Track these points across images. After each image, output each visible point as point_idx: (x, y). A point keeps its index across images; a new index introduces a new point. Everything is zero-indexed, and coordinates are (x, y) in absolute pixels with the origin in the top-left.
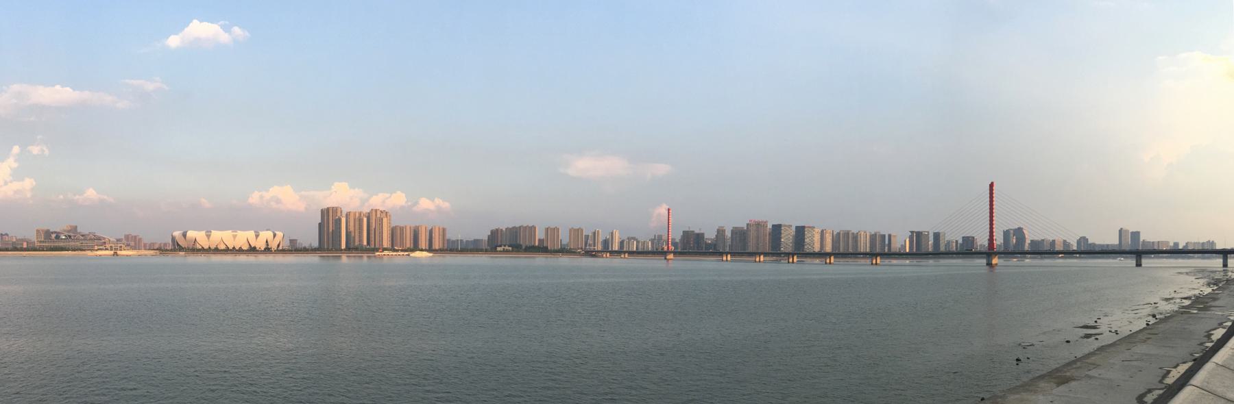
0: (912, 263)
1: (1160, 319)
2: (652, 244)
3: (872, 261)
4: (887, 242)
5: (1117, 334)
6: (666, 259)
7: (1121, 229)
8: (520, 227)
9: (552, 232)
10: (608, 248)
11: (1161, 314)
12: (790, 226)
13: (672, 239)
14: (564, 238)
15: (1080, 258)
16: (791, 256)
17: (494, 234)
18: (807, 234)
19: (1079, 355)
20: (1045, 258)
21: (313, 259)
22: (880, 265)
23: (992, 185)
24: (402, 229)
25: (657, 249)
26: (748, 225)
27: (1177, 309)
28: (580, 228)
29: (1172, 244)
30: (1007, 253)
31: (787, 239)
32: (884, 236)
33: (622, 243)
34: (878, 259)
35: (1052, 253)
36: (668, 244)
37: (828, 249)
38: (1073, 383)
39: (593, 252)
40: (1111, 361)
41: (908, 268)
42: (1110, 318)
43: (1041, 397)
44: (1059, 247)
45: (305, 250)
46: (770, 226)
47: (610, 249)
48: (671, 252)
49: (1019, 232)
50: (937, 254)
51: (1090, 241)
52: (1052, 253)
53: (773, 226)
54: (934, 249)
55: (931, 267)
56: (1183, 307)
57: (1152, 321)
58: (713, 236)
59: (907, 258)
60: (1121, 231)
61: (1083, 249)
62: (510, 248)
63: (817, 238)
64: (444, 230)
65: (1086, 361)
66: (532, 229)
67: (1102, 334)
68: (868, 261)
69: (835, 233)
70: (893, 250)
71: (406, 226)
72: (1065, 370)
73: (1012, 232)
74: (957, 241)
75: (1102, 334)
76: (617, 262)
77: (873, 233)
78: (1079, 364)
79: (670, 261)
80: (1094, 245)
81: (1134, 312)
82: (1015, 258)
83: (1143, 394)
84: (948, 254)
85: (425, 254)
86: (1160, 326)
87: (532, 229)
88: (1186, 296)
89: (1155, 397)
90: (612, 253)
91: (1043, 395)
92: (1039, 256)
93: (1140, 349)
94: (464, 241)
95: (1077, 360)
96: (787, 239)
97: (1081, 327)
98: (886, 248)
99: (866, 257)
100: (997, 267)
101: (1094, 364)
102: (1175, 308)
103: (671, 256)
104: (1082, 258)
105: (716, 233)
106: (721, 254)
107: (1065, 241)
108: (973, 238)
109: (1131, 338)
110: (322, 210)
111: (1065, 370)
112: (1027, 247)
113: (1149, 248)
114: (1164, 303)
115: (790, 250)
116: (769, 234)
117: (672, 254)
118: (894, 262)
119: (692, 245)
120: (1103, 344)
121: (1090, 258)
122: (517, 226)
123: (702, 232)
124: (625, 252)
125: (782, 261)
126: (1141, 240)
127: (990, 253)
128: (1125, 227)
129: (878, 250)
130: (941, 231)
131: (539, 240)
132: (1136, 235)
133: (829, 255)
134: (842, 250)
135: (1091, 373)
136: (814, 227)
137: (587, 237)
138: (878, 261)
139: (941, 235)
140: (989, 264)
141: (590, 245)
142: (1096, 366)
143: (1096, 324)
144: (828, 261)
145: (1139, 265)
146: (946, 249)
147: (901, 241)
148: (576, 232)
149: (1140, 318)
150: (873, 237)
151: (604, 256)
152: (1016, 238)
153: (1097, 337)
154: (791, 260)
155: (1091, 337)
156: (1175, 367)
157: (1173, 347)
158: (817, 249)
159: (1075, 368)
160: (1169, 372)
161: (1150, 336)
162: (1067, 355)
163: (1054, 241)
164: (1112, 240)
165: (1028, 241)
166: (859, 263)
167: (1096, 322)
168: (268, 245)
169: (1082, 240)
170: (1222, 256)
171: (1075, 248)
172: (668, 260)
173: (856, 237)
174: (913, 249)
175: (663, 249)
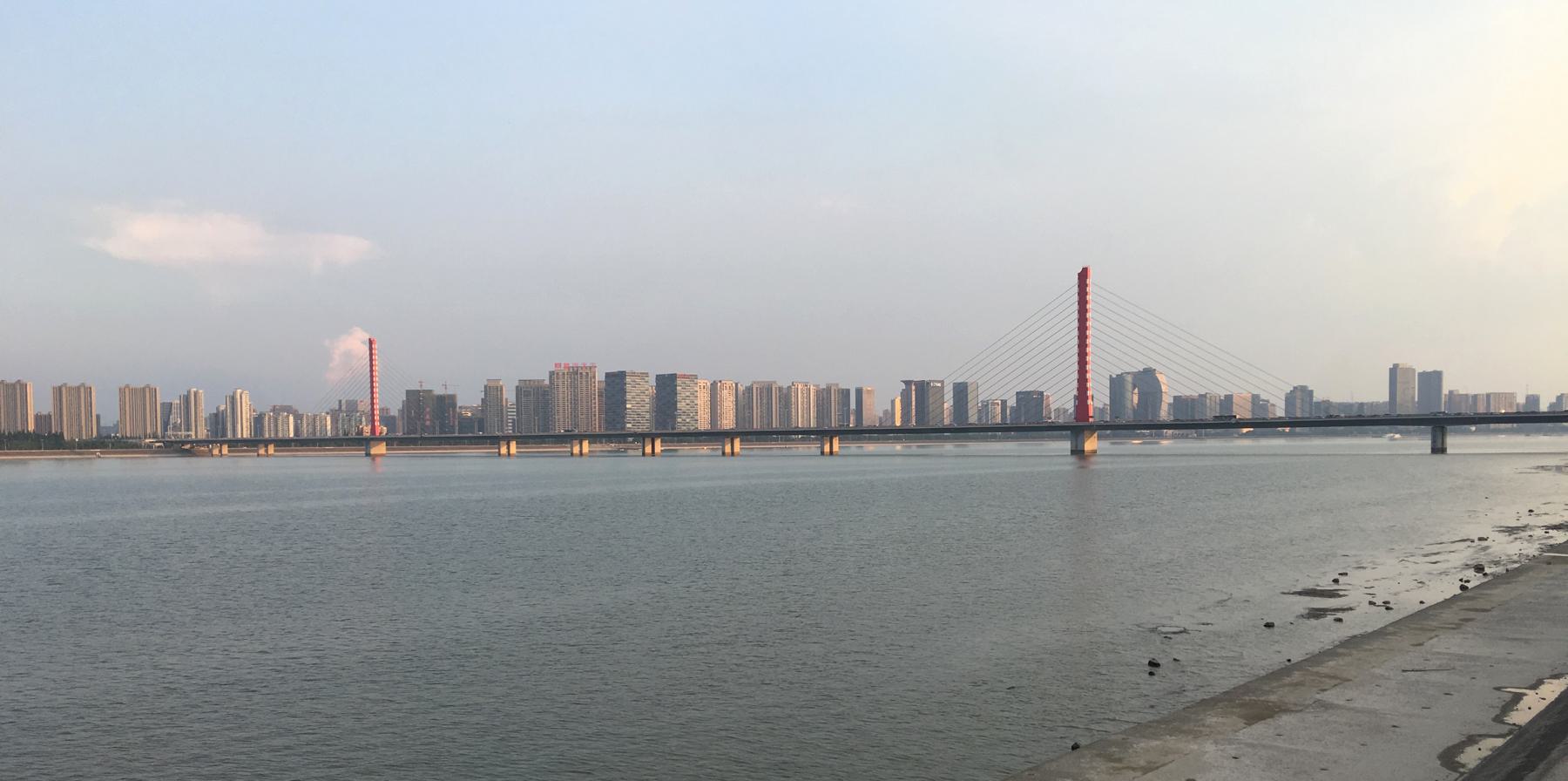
0: (908, 451)
1: (1496, 576)
2: (335, 421)
3: (822, 448)
4: (853, 406)
5: (1387, 608)
6: (368, 455)
9: (72, 396)
10: (224, 434)
11: (1497, 563)
13: (382, 410)
14: (107, 410)
16: (648, 441)
19: (1296, 657)
20: (1207, 435)
23: (1083, 276)
25: (345, 434)
26: (552, 374)
27: (1536, 553)
28: (148, 386)
29: (1521, 400)
30: (1115, 428)
31: (639, 405)
32: (848, 391)
33: (258, 421)
34: (836, 441)
35: (1226, 423)
36: (373, 421)
37: (728, 422)
38: (1285, 719)
39: (188, 442)
40: (1377, 671)
41: (898, 460)
42: (1368, 574)
43: (1210, 747)
46: (600, 376)
47: (229, 436)
48: (381, 440)
49: (1147, 380)
50: (962, 430)
51: (1318, 396)
52: (1226, 423)
53: (608, 375)
55: (948, 458)
56: (1552, 548)
57: (1475, 580)
59: (898, 440)
60: (1394, 371)
61: (1299, 414)
63: (703, 399)
65: (1315, 669)
66: (786, 397)
67: (1351, 609)
68: (814, 448)
69: (741, 388)
70: (866, 423)
72: (1266, 688)
73: (1129, 378)
75: (1351, 609)
76: (249, 465)
78: (1296, 676)
79: (379, 460)
80: (1327, 404)
81: (1427, 559)
82: (1138, 437)
83: (1454, 747)
84: (986, 431)
86: (1495, 592)
88: (1557, 521)
89: (1485, 753)
90: (235, 444)
91: (1216, 742)
92: (1193, 432)
93: (1448, 644)
95: (1289, 668)
96: (639, 405)
97: (1300, 593)
98: (852, 418)
99: (809, 439)
100: (1093, 459)
101: (1334, 677)
102: (1532, 550)
103: (380, 449)
104: (1300, 435)
105: (482, 395)
106: (495, 441)
107: (1255, 398)
108: (1041, 393)
109: (1424, 620)
111: (1266, 688)
112: (1164, 414)
113: (1465, 410)
114: (1504, 538)
115: (644, 427)
116: (206, 419)
118: (871, 448)
119: (428, 423)
120: (1357, 632)
121: (1317, 435)
123: (450, 392)
124: (266, 443)
125: (631, 452)
126: (1445, 391)
127: (1079, 426)
128: (1404, 361)
129: (834, 424)
130: (969, 381)
131: (38, 418)
132: (1432, 380)
133: (730, 435)
134: (756, 426)
135: (1330, 696)
136: (696, 377)
137: (168, 407)
138: (836, 448)
139: (970, 389)
140: (1078, 452)
141: (176, 428)
142: (1340, 680)
143: (1336, 587)
144: (728, 449)
145: (1439, 449)
146: (980, 419)
148: (137, 397)
149: (1445, 573)
150: (824, 396)
151: (216, 452)
153: (1339, 615)
154: (648, 449)
155: (1324, 615)
156: (1534, 687)
157: (1527, 641)
158: (703, 424)
159: (1291, 685)
160: (1518, 698)
161: (1471, 615)
162: (1264, 657)
163: (1229, 398)
164: (1373, 392)
165: (1167, 399)
166: (794, 451)
167: (1336, 581)
169: (1299, 394)
170: (1429, 428)
172: (374, 457)
173: (786, 397)
174: (909, 420)
175: (360, 432)
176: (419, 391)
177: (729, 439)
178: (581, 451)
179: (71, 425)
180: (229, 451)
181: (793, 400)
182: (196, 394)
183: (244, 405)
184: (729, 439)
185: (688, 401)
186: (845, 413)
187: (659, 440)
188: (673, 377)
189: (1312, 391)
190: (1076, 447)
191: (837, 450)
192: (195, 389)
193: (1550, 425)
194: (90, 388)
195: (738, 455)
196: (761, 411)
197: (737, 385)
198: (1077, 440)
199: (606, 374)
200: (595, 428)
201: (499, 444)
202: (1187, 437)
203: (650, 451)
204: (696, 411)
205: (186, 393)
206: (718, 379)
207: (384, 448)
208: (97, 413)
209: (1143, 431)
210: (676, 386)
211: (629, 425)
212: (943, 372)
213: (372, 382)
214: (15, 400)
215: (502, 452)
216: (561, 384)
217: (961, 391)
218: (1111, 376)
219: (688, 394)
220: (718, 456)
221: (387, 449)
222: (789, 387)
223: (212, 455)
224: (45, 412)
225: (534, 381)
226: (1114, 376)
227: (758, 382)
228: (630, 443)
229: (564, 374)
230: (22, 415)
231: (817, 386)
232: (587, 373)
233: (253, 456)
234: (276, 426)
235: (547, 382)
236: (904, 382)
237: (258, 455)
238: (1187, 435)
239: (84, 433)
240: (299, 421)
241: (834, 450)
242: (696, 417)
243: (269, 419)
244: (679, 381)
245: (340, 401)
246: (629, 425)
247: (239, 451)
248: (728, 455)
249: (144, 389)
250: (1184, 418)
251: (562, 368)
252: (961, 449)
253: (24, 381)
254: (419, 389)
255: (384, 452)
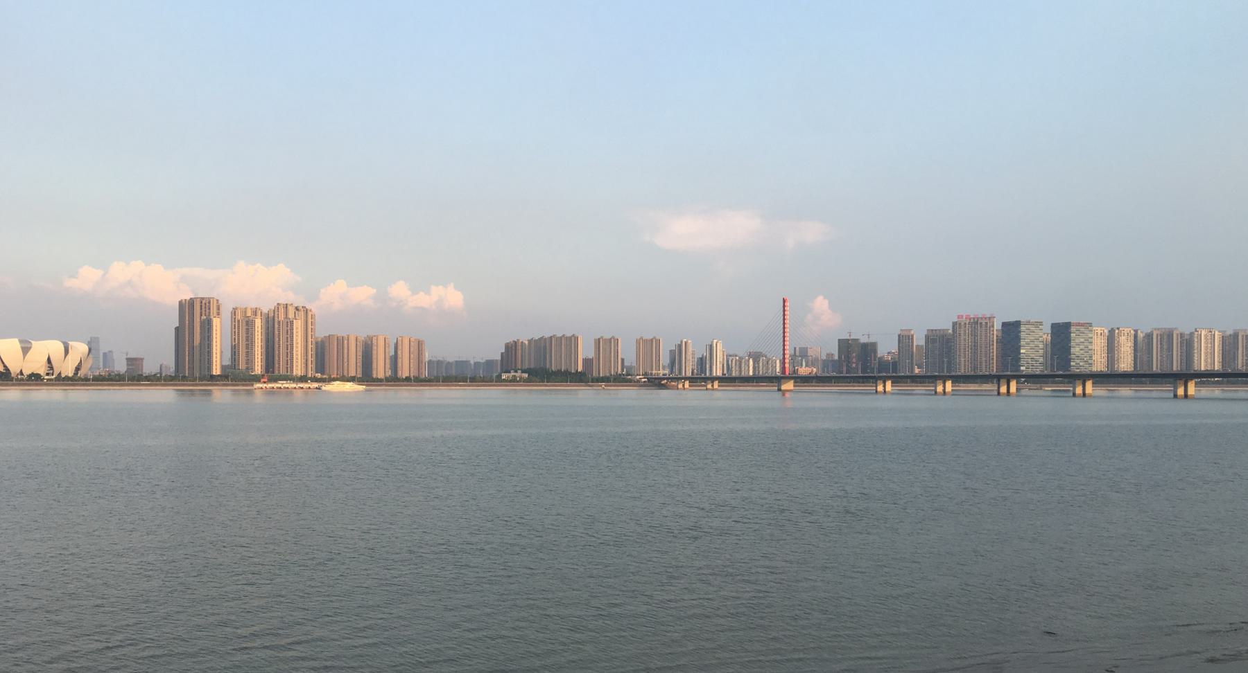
6: (779, 390)
8: (551, 337)
9: (606, 345)
12: (1038, 324)
14: (627, 354)
16: (1003, 381)
17: (511, 349)
18: (1076, 339)
21: (164, 396)
22: (1193, 398)
24: (341, 341)
26: (954, 324)
28: (613, 337)
31: (1033, 352)
34: (1089, 384)
37: (1125, 363)
39: (664, 379)
45: (135, 376)
46: (997, 326)
53: (1004, 324)
58: (895, 349)
62: (526, 375)
63: (1099, 345)
64: (420, 344)
66: (572, 341)
69: (1141, 335)
71: (348, 336)
77: (1230, 332)
85: (349, 387)
94: (472, 362)
96: (1033, 352)
103: (789, 385)
110: (180, 302)
117: (792, 381)
122: (547, 335)
123: (872, 340)
144: (1181, 391)
147: (1207, 358)
148: (649, 346)
151: (680, 386)
154: (1003, 389)
168: (52, 368)
176: (849, 340)
177: (1182, 382)
179: (605, 365)
180: (690, 386)
181: (1196, 345)
182: (686, 343)
184: (1182, 382)
185: (1082, 347)
191: (890, 390)
195: (1090, 396)
196: (1161, 356)
197: (1136, 331)
200: (993, 370)
201: (876, 381)
203: (1183, 393)
206: (1115, 326)
208: (623, 357)
210: (1070, 333)
211: (1022, 368)
213: (784, 332)
219: (1082, 340)
221: (794, 386)
222: (1192, 334)
223: (678, 389)
227: (1158, 329)
228: (1022, 383)
229: (965, 324)
232: (986, 323)
233: (704, 390)
234: (740, 367)
235: (950, 331)
236: (21, 371)
239: (612, 370)
240: (757, 365)
241: (1087, 392)
242: (1090, 361)
244: (1073, 329)
245: (795, 348)
246: (1022, 368)
247: (699, 386)
248: (1181, 398)
253: (577, 335)
254: (849, 338)
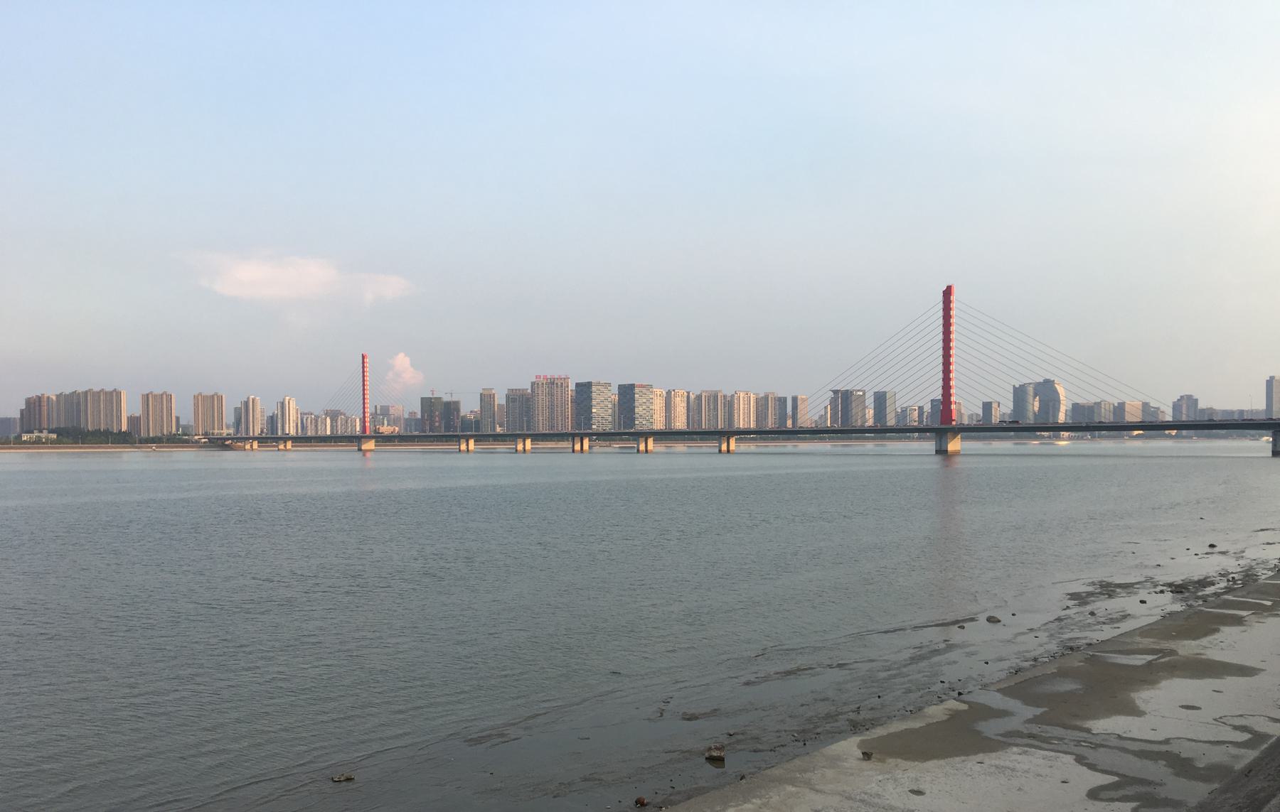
3: (720, 447)
6: (360, 450)
7: (1272, 378)
8: (86, 392)
9: (156, 402)
10: (277, 434)
14: (183, 411)
15: (919, 439)
16: (577, 440)
17: (34, 407)
18: (639, 399)
22: (734, 453)
23: (948, 293)
26: (533, 384)
28: (165, 393)
31: (603, 411)
32: (785, 399)
35: (1119, 427)
37: (680, 423)
39: (228, 439)
44: (1133, 416)
48: (370, 438)
49: (1046, 390)
50: (881, 431)
52: (1119, 427)
53: (577, 385)
54: (1072, 418)
58: (477, 408)
61: (1184, 418)
62: (54, 436)
63: (658, 404)
73: (1031, 390)
74: (921, 408)
77: (762, 395)
79: (368, 454)
80: (1211, 411)
82: (1037, 438)
87: (113, 398)
96: (603, 411)
100: (958, 459)
103: (370, 445)
117: (373, 441)
118: (804, 446)
119: (525, 419)
122: (81, 389)
123: (455, 399)
134: (704, 426)
136: (651, 386)
140: (942, 451)
144: (724, 447)
152: (1040, 401)
154: (577, 447)
158: (659, 425)
170: (1270, 432)
171: (1169, 418)
176: (431, 398)
177: (644, 439)
178: (524, 448)
180: (259, 446)
182: (253, 400)
183: (291, 409)
185: (644, 407)
186: (782, 417)
187: (473, 440)
188: (632, 387)
189: (1197, 400)
190: (941, 446)
192: (253, 397)
193: (1206, 431)
194: (171, 396)
195: (652, 452)
197: (688, 393)
198: (940, 441)
199: (576, 384)
200: (568, 429)
202: (1082, 438)
203: (726, 449)
204: (652, 414)
205: (282, 401)
206: (671, 388)
207: (374, 444)
209: (1043, 433)
212: (865, 385)
214: (112, 403)
215: (462, 449)
216: (540, 392)
217: (880, 399)
218: (1014, 386)
219: (644, 400)
220: (456, 452)
221: (376, 446)
224: (137, 415)
225: (519, 390)
226: (1017, 386)
227: (706, 391)
230: (117, 417)
231: (756, 394)
233: (275, 450)
234: (316, 426)
235: (529, 391)
236: (832, 391)
237: (279, 450)
238: (1082, 437)
241: (731, 449)
243: (311, 421)
244: (637, 390)
245: (376, 406)
246: (594, 427)
247: (268, 446)
248: (642, 452)
249: (213, 396)
250: (1084, 421)
251: (542, 379)
252: (1019, 446)
255: (373, 448)
